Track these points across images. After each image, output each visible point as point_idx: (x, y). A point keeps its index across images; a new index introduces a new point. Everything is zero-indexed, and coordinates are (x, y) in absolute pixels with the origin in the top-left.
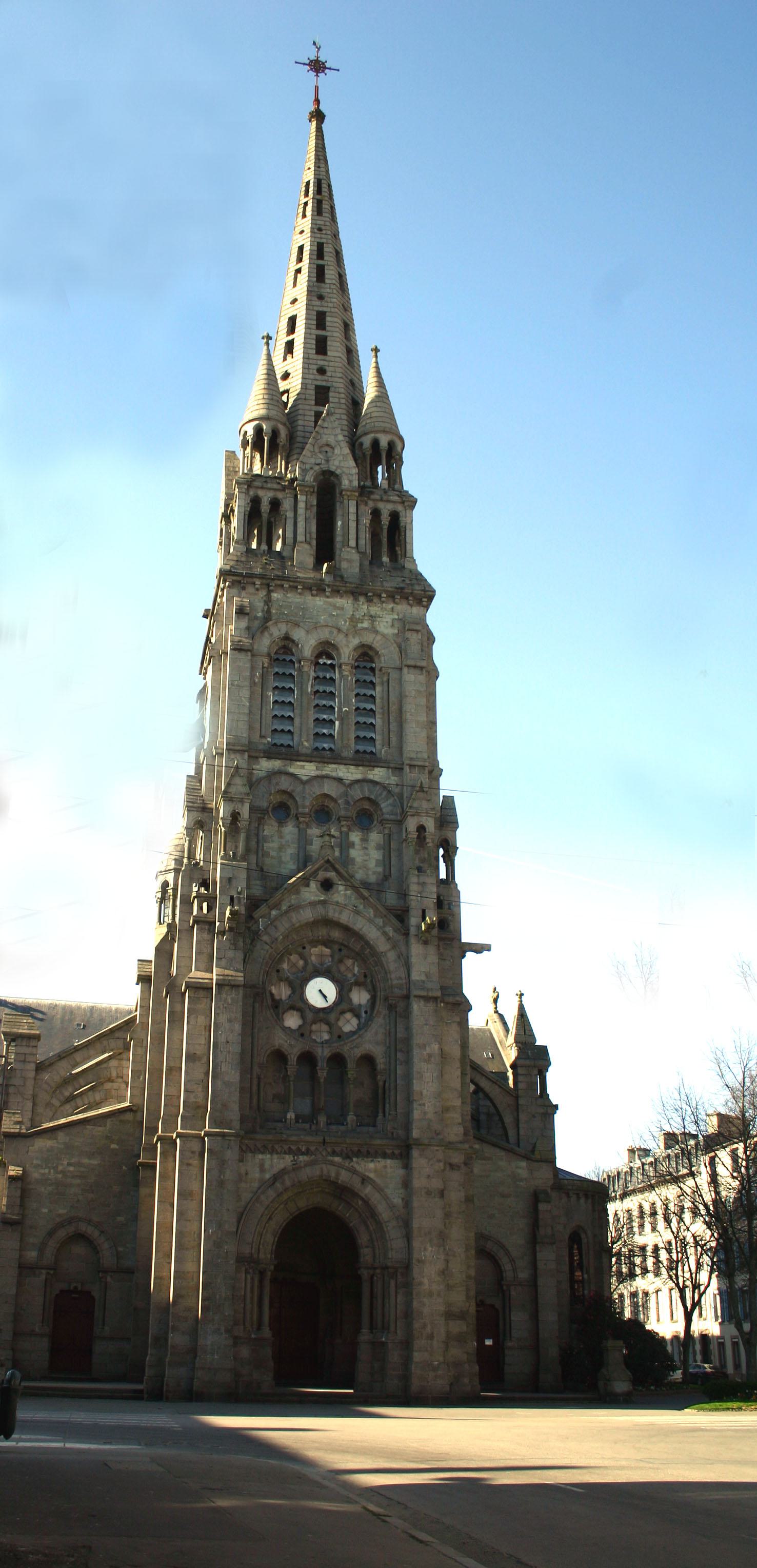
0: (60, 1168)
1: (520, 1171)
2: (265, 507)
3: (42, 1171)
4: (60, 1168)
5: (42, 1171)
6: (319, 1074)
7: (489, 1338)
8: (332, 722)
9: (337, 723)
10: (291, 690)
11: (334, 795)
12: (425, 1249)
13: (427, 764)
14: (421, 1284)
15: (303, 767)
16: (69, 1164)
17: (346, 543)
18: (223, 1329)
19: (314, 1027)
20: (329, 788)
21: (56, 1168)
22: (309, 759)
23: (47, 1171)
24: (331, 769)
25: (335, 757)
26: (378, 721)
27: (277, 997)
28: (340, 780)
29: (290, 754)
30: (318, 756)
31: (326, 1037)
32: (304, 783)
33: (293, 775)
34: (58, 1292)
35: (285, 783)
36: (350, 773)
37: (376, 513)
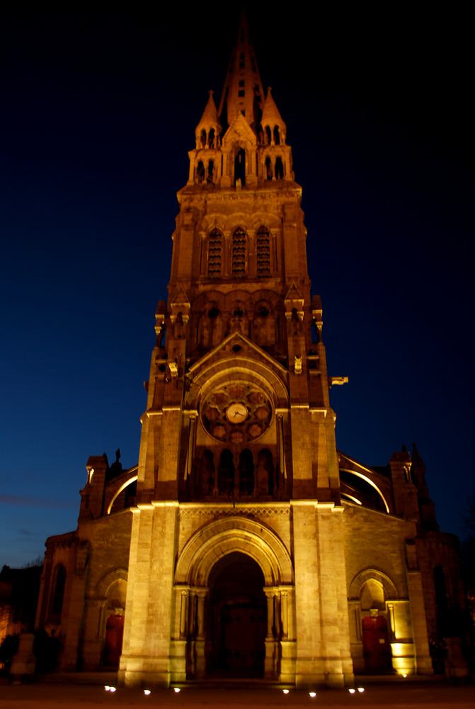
0: (110, 540)
1: (394, 528)
2: (206, 164)
3: (100, 542)
4: (110, 540)
5: (100, 542)
6: (234, 462)
7: (382, 644)
8: (244, 263)
9: (246, 263)
10: (219, 249)
11: (243, 300)
12: (304, 575)
13: (299, 275)
14: (301, 600)
15: (224, 287)
16: (116, 538)
17: (250, 171)
18: (162, 635)
19: (233, 435)
20: (240, 297)
21: (108, 541)
22: (228, 281)
23: (102, 542)
24: (242, 286)
25: (244, 280)
26: (271, 260)
27: (209, 418)
28: (247, 292)
29: (219, 281)
30: (234, 280)
31: (241, 440)
32: (225, 295)
33: (219, 292)
34: (109, 616)
35: (213, 297)
36: (254, 287)
37: (268, 160)
